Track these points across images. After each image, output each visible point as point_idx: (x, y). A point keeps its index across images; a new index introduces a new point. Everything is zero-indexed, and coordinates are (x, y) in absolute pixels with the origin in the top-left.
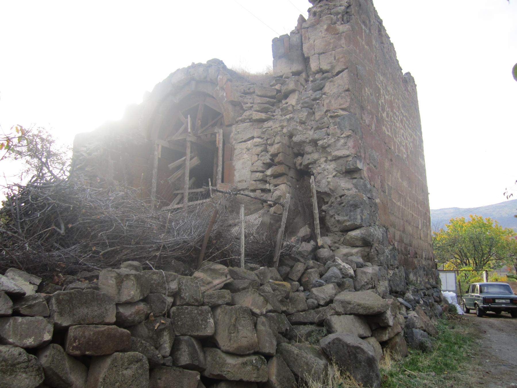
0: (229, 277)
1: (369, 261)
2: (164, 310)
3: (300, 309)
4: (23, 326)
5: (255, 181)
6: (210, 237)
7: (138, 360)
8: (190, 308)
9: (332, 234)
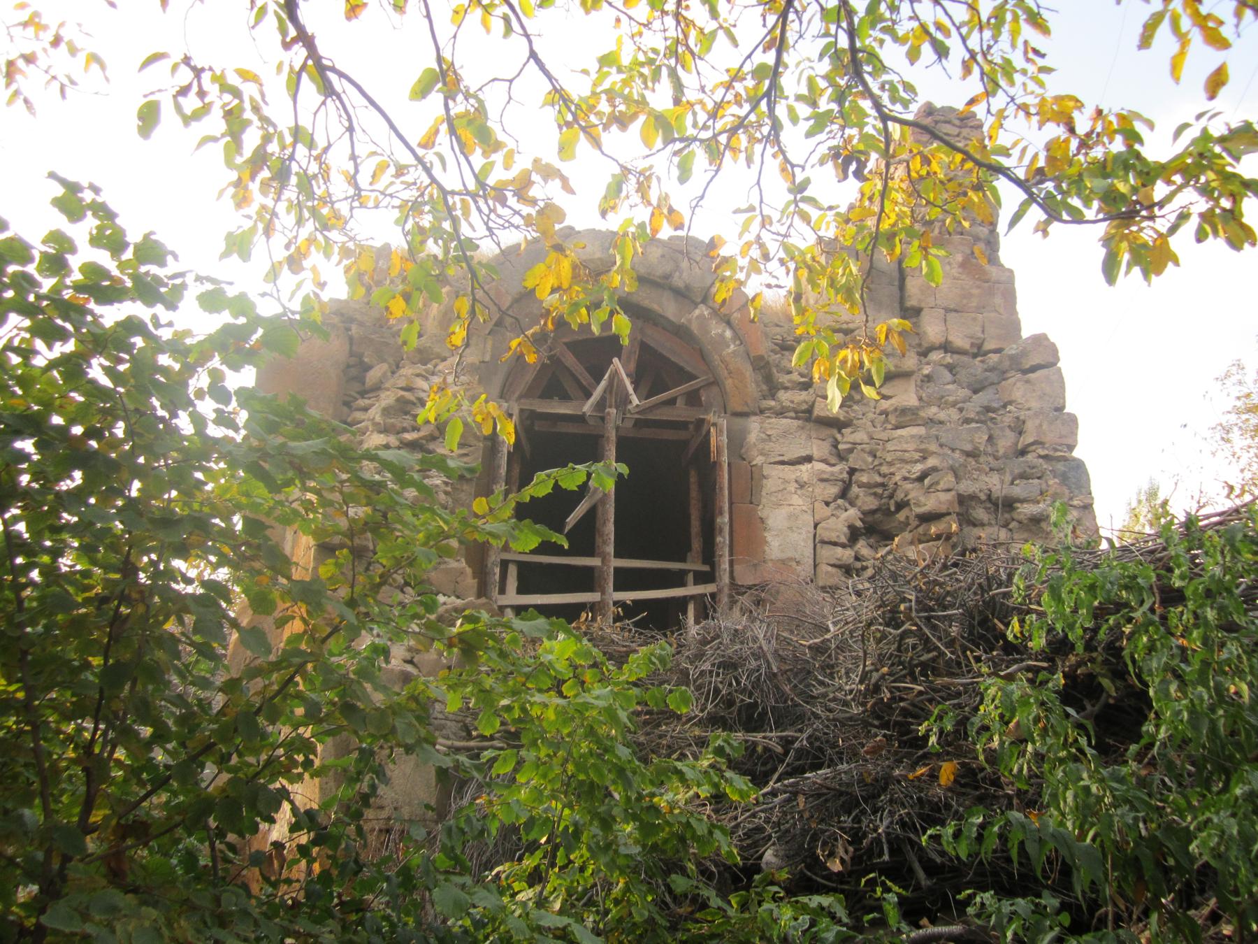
5: (833, 565)
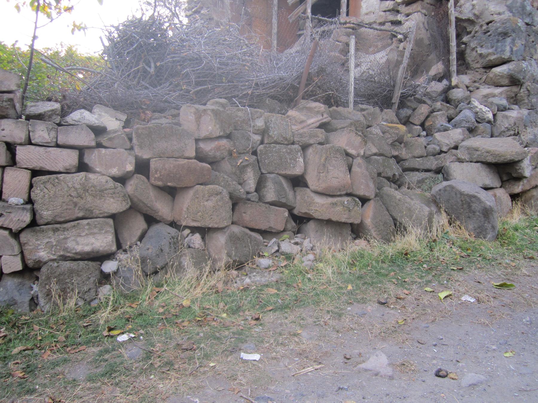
0: (325, 115)
1: (516, 104)
2: (248, 148)
3: (416, 155)
4: (107, 157)
5: (385, 11)
6: (309, 73)
7: (218, 193)
8: (278, 146)
9: (473, 72)
